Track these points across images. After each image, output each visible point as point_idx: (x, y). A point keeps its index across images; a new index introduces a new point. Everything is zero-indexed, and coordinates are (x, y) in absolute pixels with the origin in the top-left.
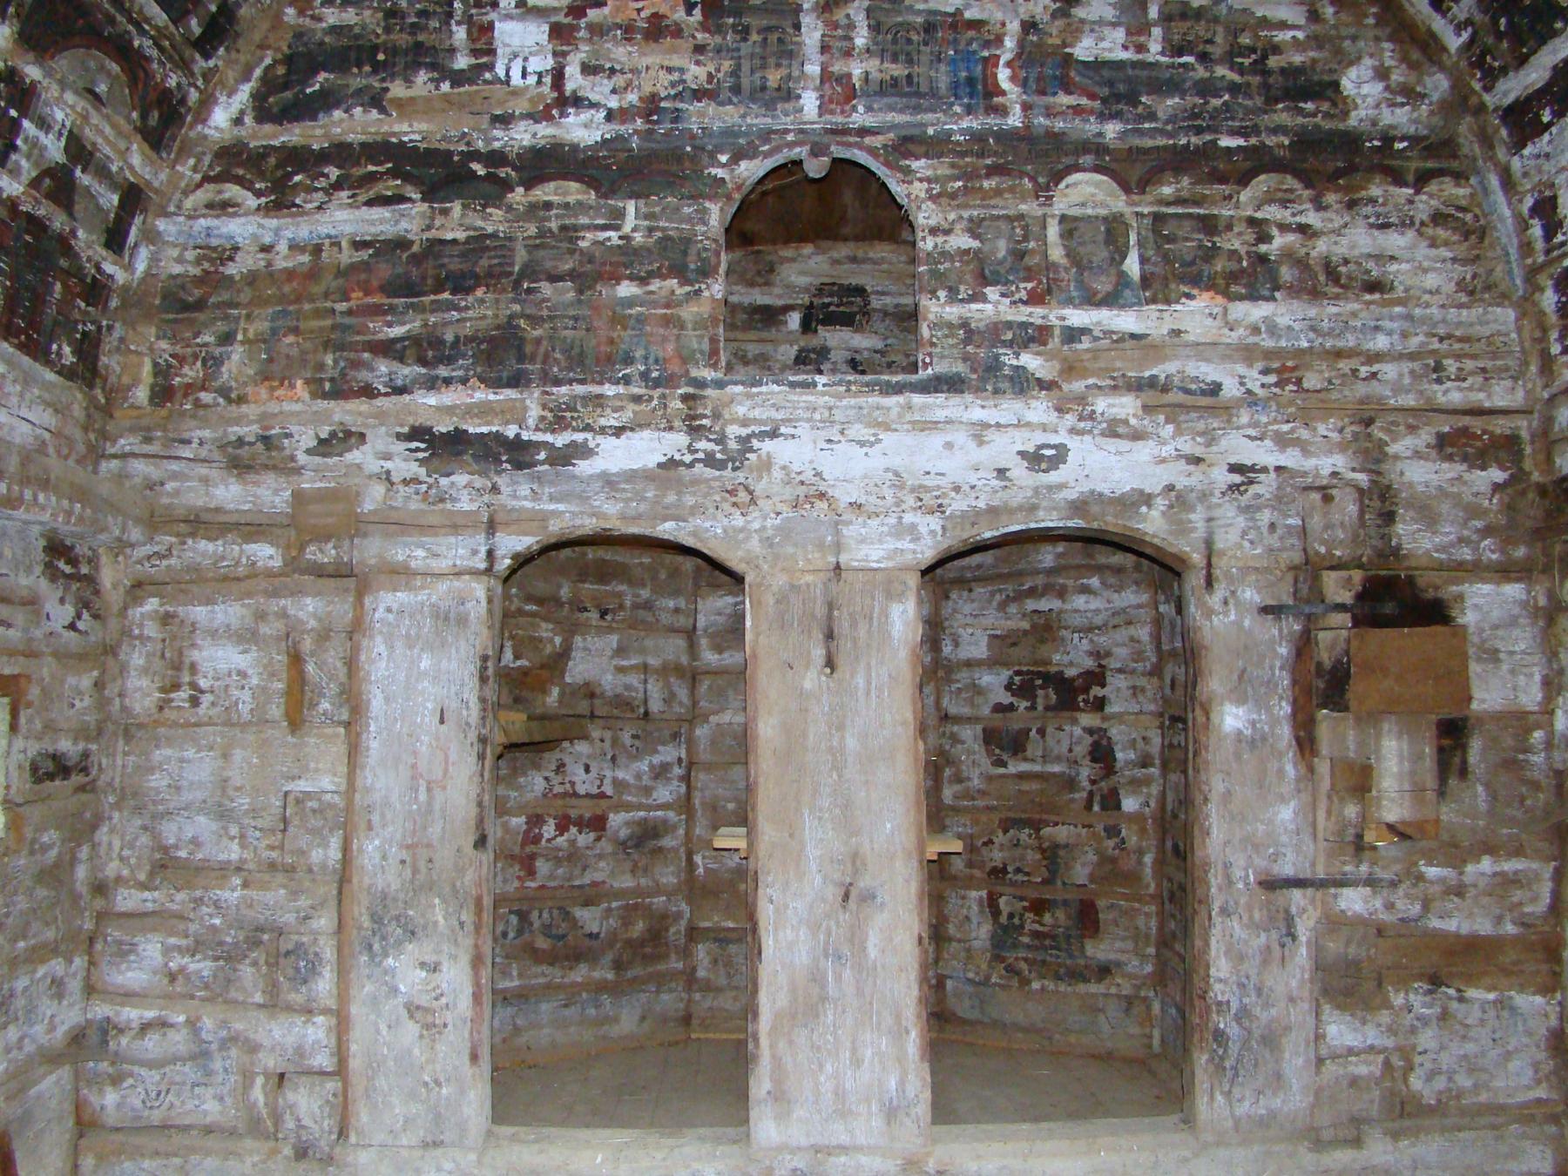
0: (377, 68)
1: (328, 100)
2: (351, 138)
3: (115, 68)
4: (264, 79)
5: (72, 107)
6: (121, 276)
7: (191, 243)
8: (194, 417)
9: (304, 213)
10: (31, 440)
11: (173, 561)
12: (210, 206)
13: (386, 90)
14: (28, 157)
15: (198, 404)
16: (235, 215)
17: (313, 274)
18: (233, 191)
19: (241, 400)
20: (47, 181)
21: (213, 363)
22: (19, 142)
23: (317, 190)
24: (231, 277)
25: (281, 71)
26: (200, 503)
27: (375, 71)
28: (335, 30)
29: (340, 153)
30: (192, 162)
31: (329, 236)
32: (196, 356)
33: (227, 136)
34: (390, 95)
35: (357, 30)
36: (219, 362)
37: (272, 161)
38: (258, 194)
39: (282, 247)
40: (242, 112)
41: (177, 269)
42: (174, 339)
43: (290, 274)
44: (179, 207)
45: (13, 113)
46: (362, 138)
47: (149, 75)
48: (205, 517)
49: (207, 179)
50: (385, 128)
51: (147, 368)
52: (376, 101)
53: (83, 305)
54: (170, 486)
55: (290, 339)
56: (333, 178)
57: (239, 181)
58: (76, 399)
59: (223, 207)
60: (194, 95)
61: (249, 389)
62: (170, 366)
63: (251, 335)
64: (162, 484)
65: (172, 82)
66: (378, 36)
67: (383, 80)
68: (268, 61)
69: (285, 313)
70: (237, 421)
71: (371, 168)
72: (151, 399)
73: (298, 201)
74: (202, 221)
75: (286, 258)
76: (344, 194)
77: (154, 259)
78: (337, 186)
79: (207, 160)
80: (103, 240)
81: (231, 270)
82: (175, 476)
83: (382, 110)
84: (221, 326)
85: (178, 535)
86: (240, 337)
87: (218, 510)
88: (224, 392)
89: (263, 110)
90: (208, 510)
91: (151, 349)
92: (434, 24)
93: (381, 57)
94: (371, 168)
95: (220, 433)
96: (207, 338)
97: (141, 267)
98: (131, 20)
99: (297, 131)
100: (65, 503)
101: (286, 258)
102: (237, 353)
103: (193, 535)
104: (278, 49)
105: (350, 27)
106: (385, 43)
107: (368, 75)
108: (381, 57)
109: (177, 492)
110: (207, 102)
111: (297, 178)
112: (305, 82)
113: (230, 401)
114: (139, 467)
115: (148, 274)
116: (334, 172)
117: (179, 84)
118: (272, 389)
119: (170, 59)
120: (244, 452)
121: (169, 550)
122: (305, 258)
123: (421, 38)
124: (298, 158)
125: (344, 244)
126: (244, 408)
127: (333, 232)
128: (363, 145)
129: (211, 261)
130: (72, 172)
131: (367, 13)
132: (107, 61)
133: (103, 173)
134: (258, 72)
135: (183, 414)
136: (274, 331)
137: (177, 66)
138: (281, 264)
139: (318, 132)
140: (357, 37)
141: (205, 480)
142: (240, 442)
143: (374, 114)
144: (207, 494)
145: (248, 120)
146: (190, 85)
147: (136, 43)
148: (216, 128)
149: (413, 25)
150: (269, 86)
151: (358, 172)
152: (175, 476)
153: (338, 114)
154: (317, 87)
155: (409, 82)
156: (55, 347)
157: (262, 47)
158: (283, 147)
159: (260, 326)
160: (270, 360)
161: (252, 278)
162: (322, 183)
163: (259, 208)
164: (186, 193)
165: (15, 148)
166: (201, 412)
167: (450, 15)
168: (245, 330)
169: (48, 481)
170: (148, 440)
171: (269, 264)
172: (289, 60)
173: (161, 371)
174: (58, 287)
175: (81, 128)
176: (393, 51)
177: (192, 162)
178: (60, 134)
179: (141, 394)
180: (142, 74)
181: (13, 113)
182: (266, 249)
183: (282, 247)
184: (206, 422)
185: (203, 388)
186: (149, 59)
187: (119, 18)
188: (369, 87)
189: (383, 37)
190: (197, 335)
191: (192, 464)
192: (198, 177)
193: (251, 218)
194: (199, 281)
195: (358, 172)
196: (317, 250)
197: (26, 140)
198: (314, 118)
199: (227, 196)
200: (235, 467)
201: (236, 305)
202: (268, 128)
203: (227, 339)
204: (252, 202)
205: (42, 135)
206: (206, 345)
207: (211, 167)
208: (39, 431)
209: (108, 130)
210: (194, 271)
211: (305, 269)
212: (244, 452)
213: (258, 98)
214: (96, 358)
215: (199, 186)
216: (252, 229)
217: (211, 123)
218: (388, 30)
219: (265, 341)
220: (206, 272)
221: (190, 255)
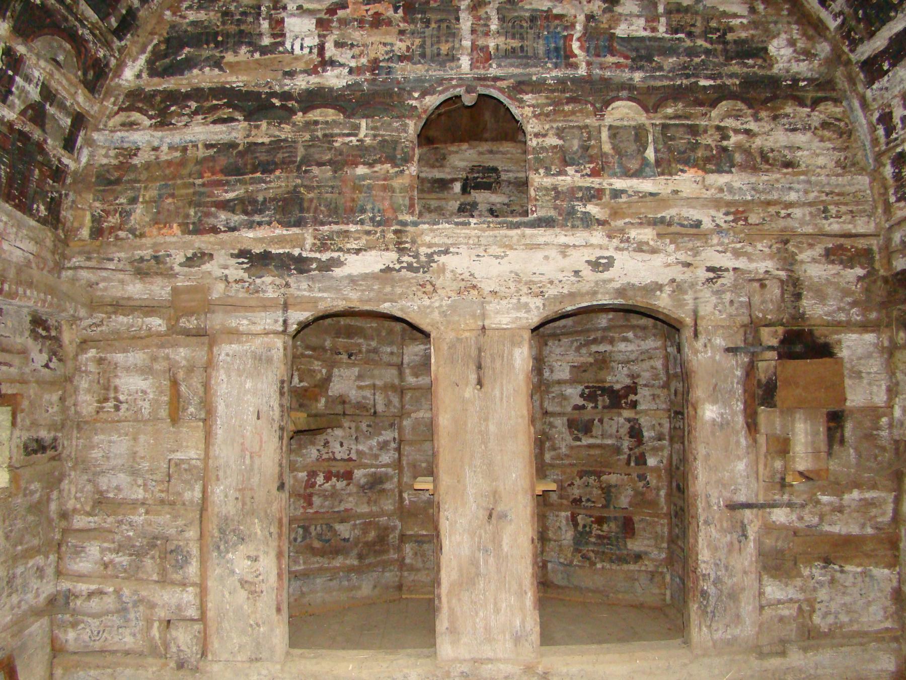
0: (218, 45)
1: (190, 64)
2: (203, 85)
3: (68, 46)
4: (153, 52)
5: (44, 69)
6: (72, 166)
7: (113, 146)
8: (115, 245)
9: (177, 129)
10: (22, 259)
11: (104, 328)
12: (123, 125)
13: (223, 57)
14: (19, 98)
15: (117, 238)
16: (137, 130)
17: (182, 163)
18: (136, 116)
19: (142, 235)
20: (30, 111)
21: (126, 214)
22: (14, 89)
23: (184, 115)
24: (135, 165)
25: (163, 47)
26: (119, 295)
27: (217, 47)
28: (193, 23)
29: (197, 94)
30: (112, 99)
31: (191, 142)
32: (116, 211)
33: (132, 85)
34: (225, 60)
35: (206, 23)
36: (129, 214)
37: (158, 99)
38: (151, 118)
39: (165, 148)
40: (141, 71)
41: (105, 161)
42: (103, 201)
43: (169, 163)
44: (105, 126)
45: (10, 73)
46: (210, 85)
47: (87, 50)
48: (122, 302)
49: (121, 109)
50: (223, 79)
51: (88, 218)
52: (217, 64)
53: (51, 182)
54: (102, 285)
55: (170, 200)
56: (193, 108)
57: (140, 110)
58: (48, 236)
59: (131, 125)
60: (113, 62)
61: (147, 229)
62: (101, 216)
63: (147, 198)
64: (97, 284)
65: (101, 54)
66: (218, 27)
67: (221, 52)
68: (155, 42)
69: (166, 186)
70: (140, 248)
71: (215, 102)
72: (91, 235)
73: (173, 121)
74: (119, 133)
75: (167, 154)
76: (200, 117)
77: (92, 156)
78: (196, 113)
79: (121, 98)
80: (62, 145)
81: (136, 161)
82: (104, 279)
83: (221, 69)
84: (130, 194)
85: (106, 313)
86: (141, 200)
87: (129, 298)
88: (132, 231)
89: (153, 70)
90: (123, 298)
91: (90, 207)
92: (250, 19)
93: (220, 39)
94: (215, 102)
95: (130, 254)
96: (122, 200)
97: (84, 160)
98: (77, 19)
99: (172, 81)
100: (42, 295)
101: (167, 154)
102: (139, 209)
103: (115, 313)
104: (161, 35)
105: (202, 22)
106: (222, 30)
107: (212, 49)
108: (220, 39)
109: (106, 289)
110: (121, 66)
111: (173, 108)
112: (177, 53)
113: (135, 236)
114: (84, 274)
115: (88, 164)
116: (194, 105)
117: (105, 55)
118: (160, 229)
119: (100, 41)
120: (144, 265)
121: (102, 321)
122: (178, 154)
123: (243, 27)
124: (173, 97)
125: (200, 146)
126: (144, 240)
127: (194, 139)
128: (210, 89)
129: (124, 156)
130: (44, 106)
131: (212, 14)
132: (64, 43)
133: (62, 107)
134: (150, 48)
135: (109, 244)
136: (160, 196)
137: (104, 45)
138: (164, 157)
139: (185, 82)
140: (206, 27)
141: (122, 282)
142: (142, 259)
143: (216, 71)
144: (123, 289)
145: (145, 75)
146: (111, 55)
147: (80, 32)
148: (126, 80)
149: (238, 20)
150: (156, 55)
151: (207, 104)
152: (104, 279)
153: (195, 71)
154: (184, 56)
155: (236, 53)
156: (35, 206)
157: (152, 33)
158: (165, 91)
159: (152, 193)
160: (158, 213)
161: (147, 166)
162: (187, 111)
163: (151, 126)
164: (109, 117)
165: (11, 93)
166: (119, 243)
167: (259, 14)
168: (144, 196)
169: (32, 283)
170: (89, 259)
171: (157, 158)
172: (167, 41)
173: (96, 220)
174: (37, 172)
175: (49, 81)
176: (227, 35)
177: (112, 99)
178: (37, 85)
179: (85, 233)
180: (83, 49)
181: (10, 73)
182: (155, 149)
183: (165, 148)
184: (121, 249)
185: (120, 229)
186: (87, 41)
187: (70, 18)
188: (213, 56)
189: (221, 27)
190: (116, 199)
191: (114, 273)
192: (116, 108)
193: (146, 131)
194: (118, 168)
195: (207, 104)
196: (185, 149)
197: (18, 88)
198: (182, 74)
199: (132, 119)
200: (139, 274)
201: (139, 181)
202: (156, 80)
203: (133, 201)
204: (147, 122)
205: (27, 85)
206: (121, 204)
207: (123, 102)
208: (27, 254)
209: (64, 82)
210: (115, 162)
211: (178, 160)
212: (144, 265)
213: (150, 63)
214: (59, 212)
215: (117, 113)
216: (147, 138)
217: (123, 77)
218: (224, 23)
219: (155, 202)
220: (122, 163)
221: (112, 153)
